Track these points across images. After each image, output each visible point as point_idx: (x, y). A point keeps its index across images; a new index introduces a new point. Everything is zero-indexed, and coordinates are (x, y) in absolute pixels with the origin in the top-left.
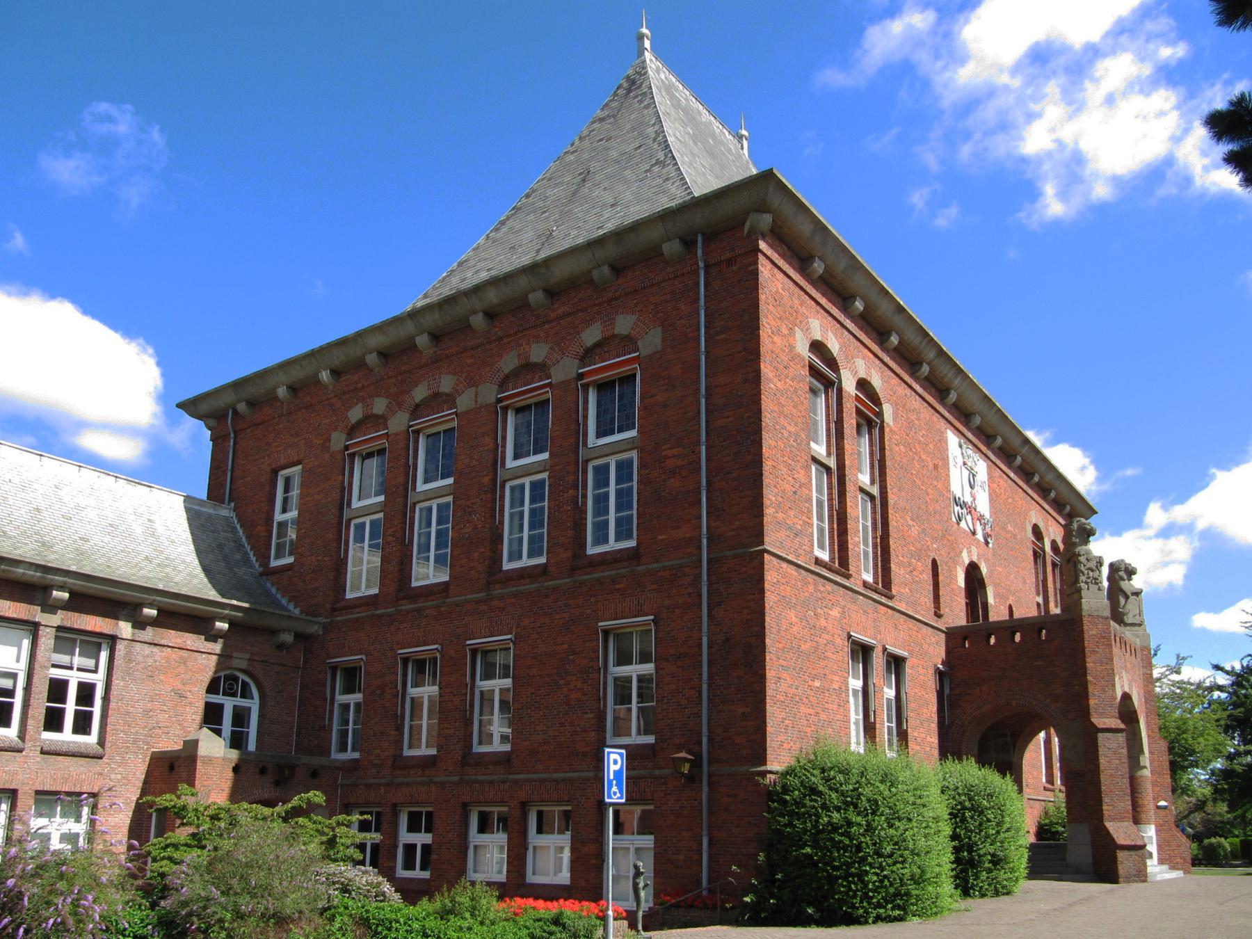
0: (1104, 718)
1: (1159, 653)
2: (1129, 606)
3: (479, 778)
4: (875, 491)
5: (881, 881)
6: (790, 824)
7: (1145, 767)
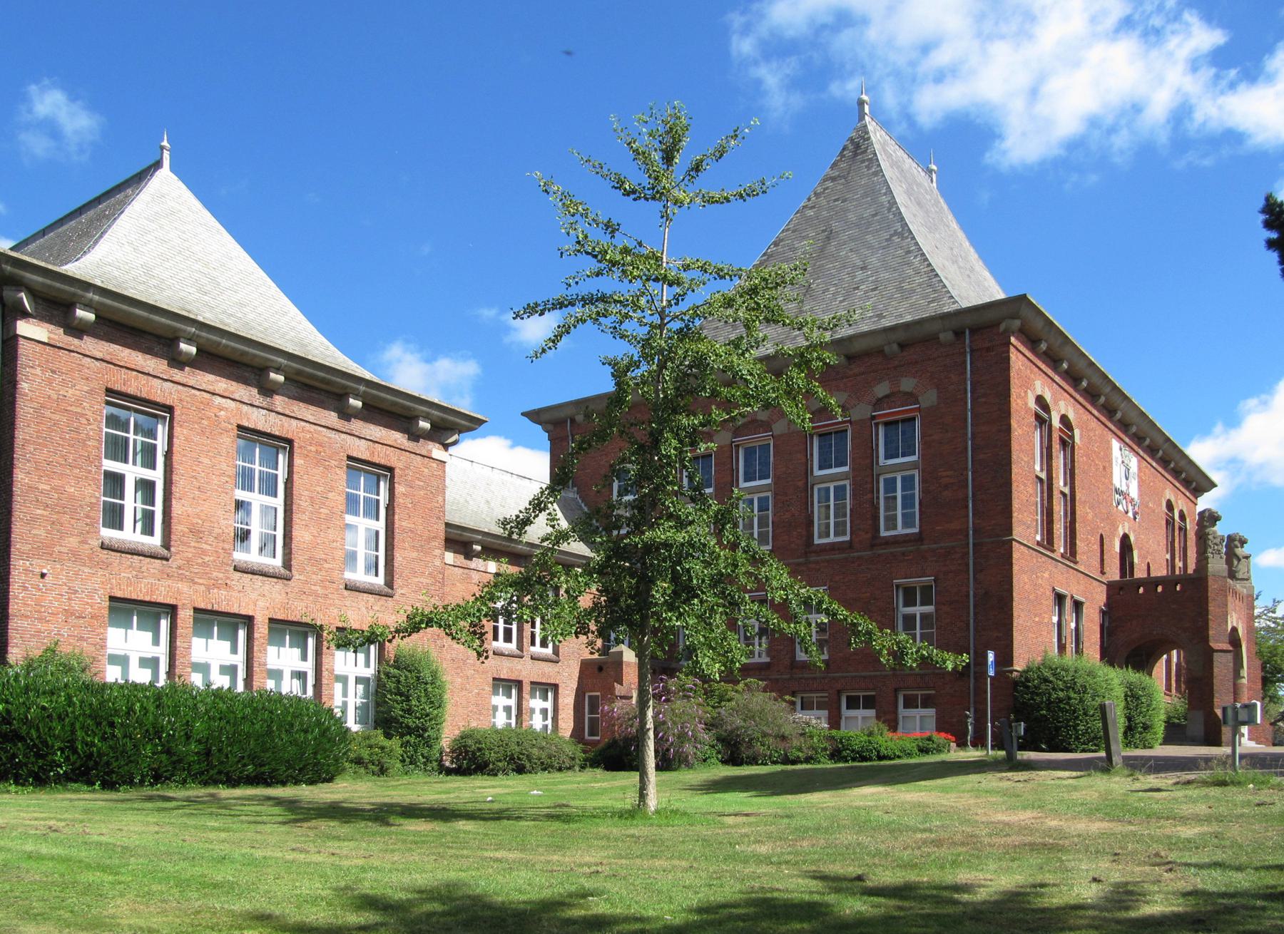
0: (1218, 643)
1: (1260, 597)
2: (1240, 566)
3: (806, 676)
4: (1043, 476)
5: (1087, 730)
6: (1033, 699)
7: (1244, 677)
